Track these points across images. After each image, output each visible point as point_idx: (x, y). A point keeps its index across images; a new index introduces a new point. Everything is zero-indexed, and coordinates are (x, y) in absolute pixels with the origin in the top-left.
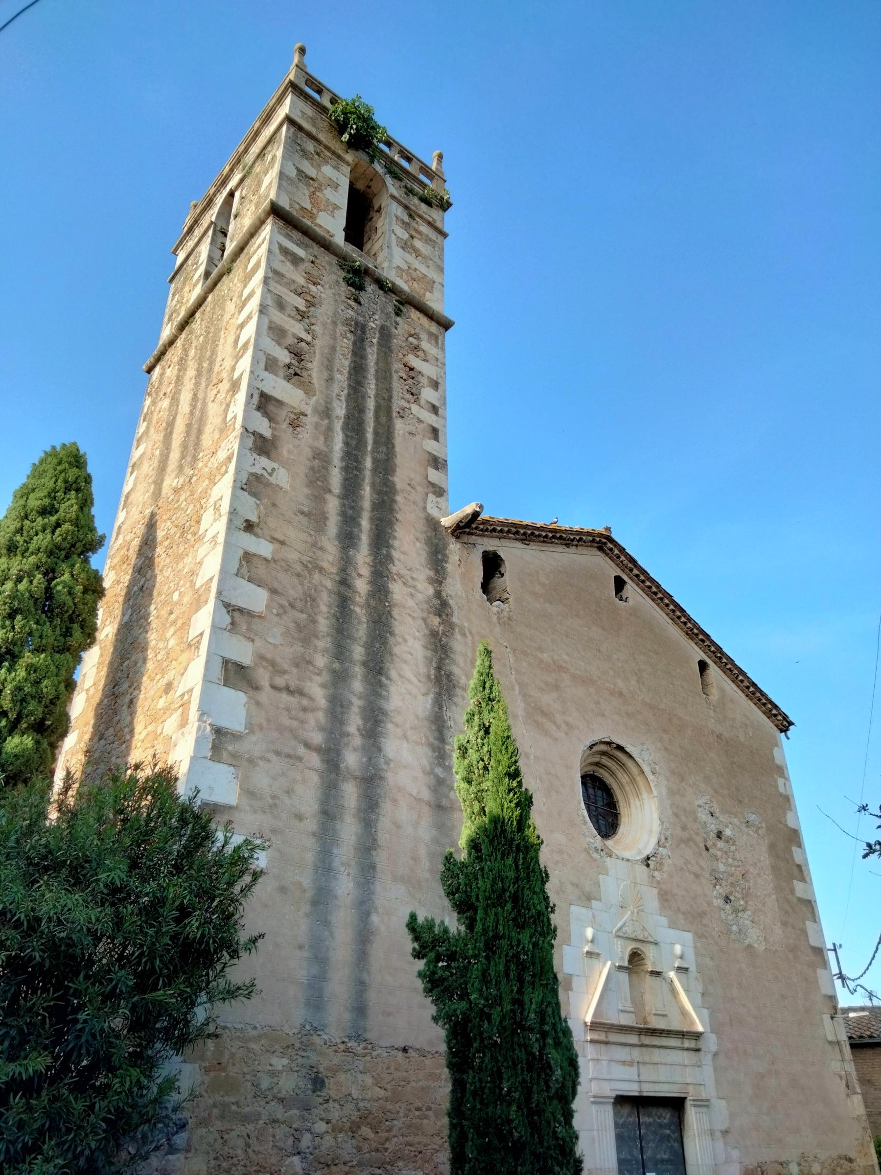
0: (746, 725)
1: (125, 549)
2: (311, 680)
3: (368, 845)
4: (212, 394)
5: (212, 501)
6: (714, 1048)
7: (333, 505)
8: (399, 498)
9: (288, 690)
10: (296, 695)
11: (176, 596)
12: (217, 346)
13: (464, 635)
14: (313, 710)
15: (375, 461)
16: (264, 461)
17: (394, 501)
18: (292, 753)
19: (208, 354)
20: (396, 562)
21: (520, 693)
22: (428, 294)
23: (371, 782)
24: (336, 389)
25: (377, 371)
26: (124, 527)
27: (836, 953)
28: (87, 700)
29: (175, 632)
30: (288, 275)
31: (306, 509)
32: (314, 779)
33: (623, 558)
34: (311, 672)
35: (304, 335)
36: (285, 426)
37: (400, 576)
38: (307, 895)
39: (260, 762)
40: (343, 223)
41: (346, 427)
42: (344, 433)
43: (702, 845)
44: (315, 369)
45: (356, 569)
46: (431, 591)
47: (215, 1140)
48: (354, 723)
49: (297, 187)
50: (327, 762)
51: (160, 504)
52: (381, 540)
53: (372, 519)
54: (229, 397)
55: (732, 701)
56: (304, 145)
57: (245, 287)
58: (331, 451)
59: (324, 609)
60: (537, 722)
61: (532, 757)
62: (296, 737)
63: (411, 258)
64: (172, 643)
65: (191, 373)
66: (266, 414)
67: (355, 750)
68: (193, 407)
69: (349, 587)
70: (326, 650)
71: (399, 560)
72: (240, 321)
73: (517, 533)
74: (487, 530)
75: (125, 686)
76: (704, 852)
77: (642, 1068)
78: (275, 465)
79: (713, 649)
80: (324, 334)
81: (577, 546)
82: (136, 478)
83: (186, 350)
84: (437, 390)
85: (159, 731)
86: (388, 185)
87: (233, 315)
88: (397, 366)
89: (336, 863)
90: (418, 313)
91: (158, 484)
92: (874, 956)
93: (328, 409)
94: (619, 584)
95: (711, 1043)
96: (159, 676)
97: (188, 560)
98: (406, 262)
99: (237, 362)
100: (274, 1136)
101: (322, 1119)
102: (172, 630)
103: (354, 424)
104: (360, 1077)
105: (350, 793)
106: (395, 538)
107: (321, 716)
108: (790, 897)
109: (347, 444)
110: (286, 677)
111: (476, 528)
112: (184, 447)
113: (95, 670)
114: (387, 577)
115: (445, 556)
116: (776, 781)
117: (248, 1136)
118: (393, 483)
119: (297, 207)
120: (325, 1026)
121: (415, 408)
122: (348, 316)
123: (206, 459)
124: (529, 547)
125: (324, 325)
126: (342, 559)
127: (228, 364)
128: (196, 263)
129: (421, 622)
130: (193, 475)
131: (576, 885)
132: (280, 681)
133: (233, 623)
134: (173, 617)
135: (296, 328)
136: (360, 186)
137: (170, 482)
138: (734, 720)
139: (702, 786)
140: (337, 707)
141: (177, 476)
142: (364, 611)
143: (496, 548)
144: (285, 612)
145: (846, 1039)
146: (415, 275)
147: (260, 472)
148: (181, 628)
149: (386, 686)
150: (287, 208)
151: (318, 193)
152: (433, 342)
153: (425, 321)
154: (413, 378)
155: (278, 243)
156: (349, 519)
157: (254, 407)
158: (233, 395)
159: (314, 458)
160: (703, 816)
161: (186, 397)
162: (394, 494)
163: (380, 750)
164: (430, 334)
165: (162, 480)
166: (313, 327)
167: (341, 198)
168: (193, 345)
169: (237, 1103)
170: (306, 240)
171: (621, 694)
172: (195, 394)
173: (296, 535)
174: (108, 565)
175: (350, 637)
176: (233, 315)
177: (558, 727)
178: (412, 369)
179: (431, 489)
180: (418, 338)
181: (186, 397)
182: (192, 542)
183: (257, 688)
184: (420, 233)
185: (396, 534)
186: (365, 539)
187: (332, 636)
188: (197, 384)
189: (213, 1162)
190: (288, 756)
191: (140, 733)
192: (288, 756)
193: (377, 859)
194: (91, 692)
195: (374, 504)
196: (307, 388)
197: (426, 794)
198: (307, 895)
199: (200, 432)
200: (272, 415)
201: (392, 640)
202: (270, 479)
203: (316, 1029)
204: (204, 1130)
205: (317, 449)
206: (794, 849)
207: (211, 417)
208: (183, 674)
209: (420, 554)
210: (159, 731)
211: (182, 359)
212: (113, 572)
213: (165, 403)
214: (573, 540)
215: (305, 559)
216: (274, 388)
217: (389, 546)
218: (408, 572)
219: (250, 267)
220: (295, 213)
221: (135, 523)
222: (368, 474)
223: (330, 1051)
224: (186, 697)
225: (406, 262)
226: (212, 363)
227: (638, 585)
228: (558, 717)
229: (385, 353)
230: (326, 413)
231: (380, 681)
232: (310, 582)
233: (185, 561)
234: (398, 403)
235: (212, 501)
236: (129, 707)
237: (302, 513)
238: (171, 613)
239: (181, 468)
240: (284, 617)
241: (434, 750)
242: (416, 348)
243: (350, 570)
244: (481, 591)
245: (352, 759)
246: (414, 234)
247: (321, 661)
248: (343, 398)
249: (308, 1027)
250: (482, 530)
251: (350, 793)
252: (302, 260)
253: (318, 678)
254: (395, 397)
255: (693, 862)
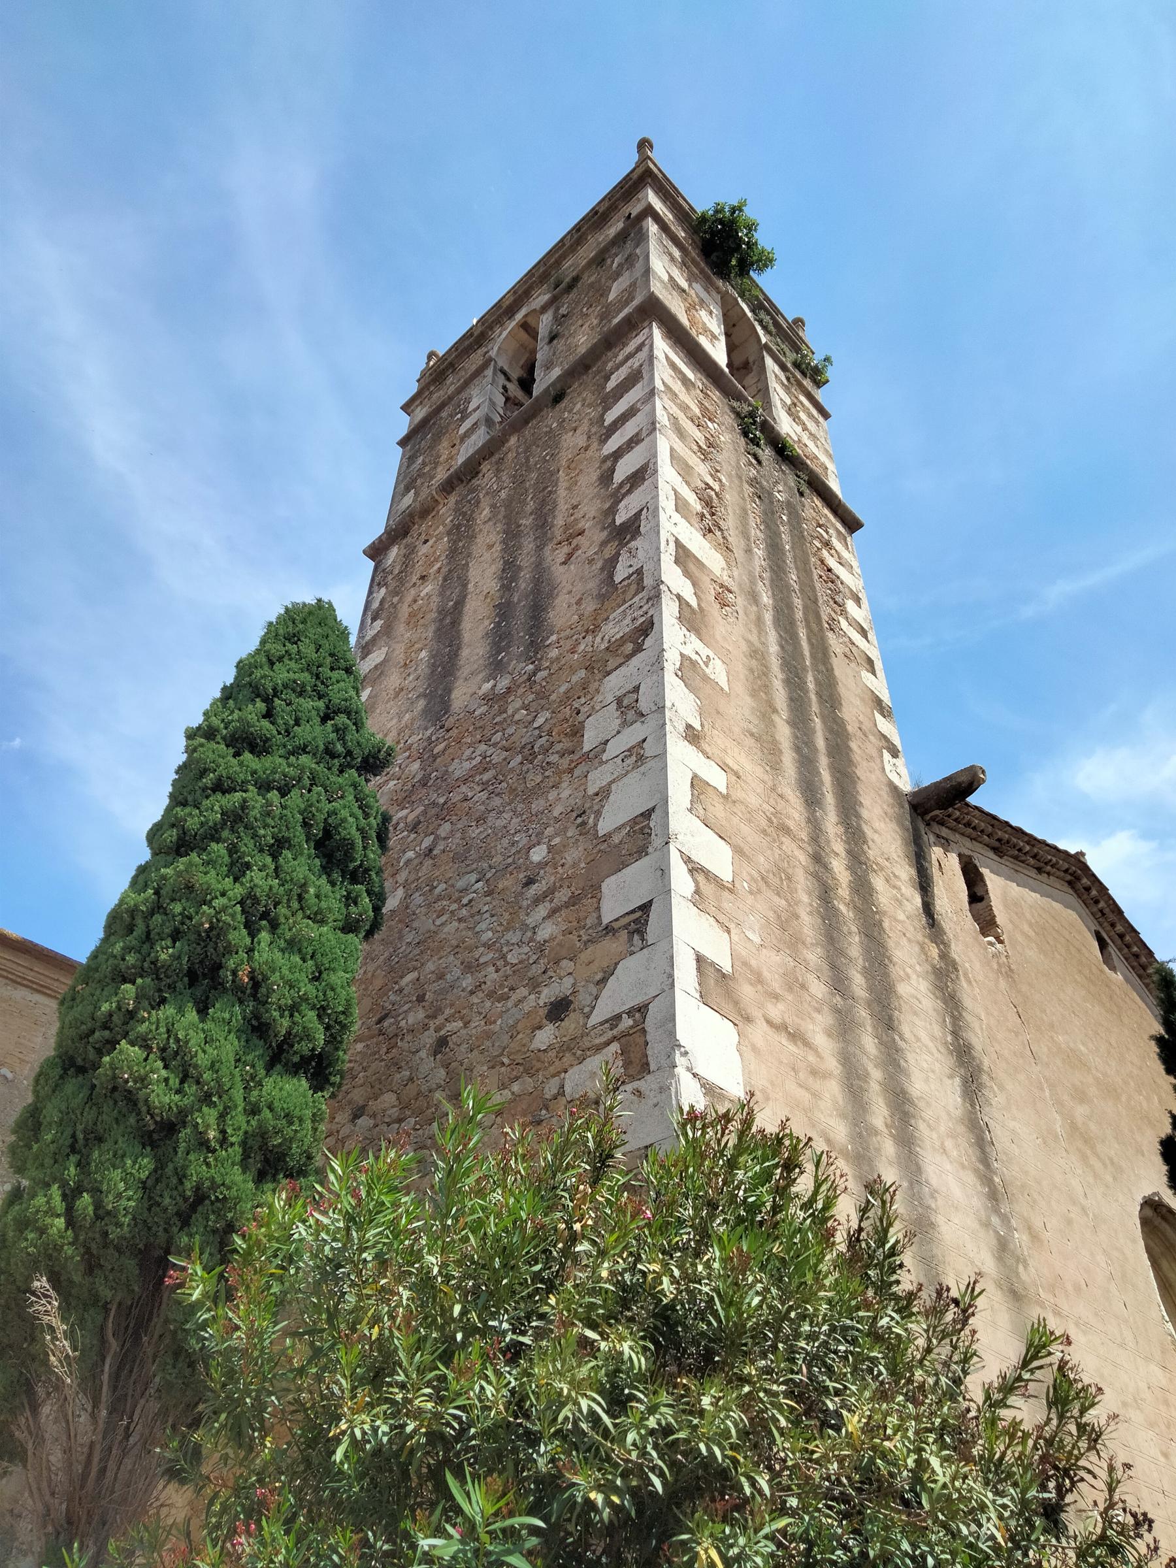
7: (784, 733)
20: (870, 843)
25: (795, 557)
41: (777, 621)
48: (880, 1115)
59: (805, 898)
90: (818, 502)
124: (1002, 861)
129: (917, 949)
133: (697, 892)
149: (902, 1050)
156: (806, 763)
174: (450, 1117)
183: (748, 1019)
186: (830, 799)
187: (822, 946)
202: (707, 671)
227: (1120, 950)
234: (825, 612)
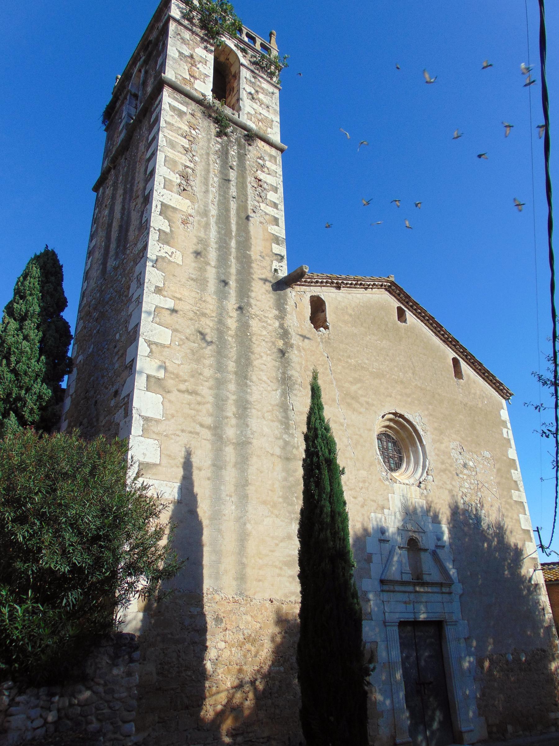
0: (483, 397)
1: (87, 307)
2: (202, 385)
3: (243, 484)
4: (133, 205)
5: (135, 275)
6: (460, 592)
8: (254, 265)
9: (187, 391)
10: (194, 395)
11: (117, 336)
12: (135, 173)
13: (300, 351)
14: (204, 404)
15: (238, 243)
16: (167, 248)
17: (251, 267)
18: (193, 430)
19: (130, 179)
20: (254, 307)
21: (336, 385)
22: (269, 130)
23: (243, 444)
24: (211, 196)
26: (87, 292)
27: (539, 532)
28: (72, 401)
29: (118, 358)
30: (176, 124)
31: (193, 276)
32: (208, 446)
33: (402, 295)
34: (202, 380)
35: (188, 164)
36: (179, 223)
37: (257, 316)
38: (207, 515)
39: (173, 436)
40: (211, 86)
42: (217, 225)
43: (454, 473)
44: (197, 184)
45: (228, 313)
46: (277, 324)
47: (160, 654)
48: (231, 409)
49: (179, 64)
50: (214, 435)
51: (106, 278)
52: (244, 291)
53: (237, 281)
54: (143, 207)
55: (474, 382)
56: (182, 35)
57: (150, 134)
58: (209, 238)
60: (349, 405)
61: (345, 425)
62: (194, 421)
63: (255, 106)
64: (117, 366)
65: (120, 191)
66: (166, 218)
67: (232, 427)
68: (123, 214)
69: (224, 325)
70: (211, 366)
71: (255, 305)
72: (148, 156)
73: (332, 283)
74: (312, 283)
75: (92, 393)
76: (456, 477)
77: (415, 605)
78: (174, 250)
79: (454, 343)
80: (201, 161)
81: (372, 289)
82: (92, 261)
83: (117, 177)
84: (277, 193)
85: (112, 420)
86: (240, 57)
87: (143, 153)
88: (250, 179)
89: (223, 495)
90: (262, 143)
91: (104, 264)
92: (553, 531)
93: (205, 210)
94: (401, 314)
95: (458, 588)
96: (111, 386)
97: (123, 313)
98: (254, 109)
99: (146, 184)
100: (194, 651)
101: (222, 641)
102: (116, 358)
103: (223, 219)
104: (244, 617)
105: (230, 453)
106: (252, 291)
107: (209, 406)
108: (509, 500)
109: (219, 233)
110: (187, 384)
111: (305, 282)
112: (119, 240)
113: (74, 383)
114: (248, 317)
115: (286, 300)
116: (502, 430)
117: (179, 651)
118: (250, 256)
119: (180, 78)
120: (221, 589)
121: (263, 206)
122: (217, 149)
123: (131, 248)
125: (201, 155)
126: (219, 307)
127: (141, 185)
128: (121, 118)
130: (124, 258)
131: (374, 501)
132: (183, 387)
133: (151, 352)
134: (116, 350)
135: (184, 160)
136: (222, 59)
137: (111, 263)
138: (475, 394)
139: (454, 436)
140: (219, 404)
141: (115, 260)
142: (234, 340)
143: (319, 294)
144: (184, 343)
145: (544, 582)
146: (260, 117)
147: (164, 255)
148: (121, 356)
150: (174, 79)
151: (194, 68)
152: (273, 161)
153: (267, 147)
154: (261, 186)
155: (169, 104)
157: (158, 213)
158: (145, 206)
159: (198, 243)
160: (454, 454)
161: (118, 208)
162: (251, 263)
163: (247, 426)
164: (271, 156)
165: (107, 263)
166: (194, 157)
167: (209, 70)
168: (121, 173)
169: (172, 634)
170: (187, 100)
171: (402, 382)
172: (123, 206)
173: (188, 294)
175: (226, 356)
176: (143, 153)
177: (362, 405)
178: (260, 180)
179: (275, 257)
180: (264, 160)
181: (118, 208)
182: (125, 302)
184: (262, 89)
185: (252, 289)
188: (124, 199)
189: (159, 666)
190: (191, 432)
191: (102, 422)
192: (191, 432)
193: (248, 492)
194: (74, 397)
195: (237, 270)
196: (192, 198)
197: (278, 451)
198: (207, 515)
199: (127, 230)
200: (170, 218)
201: (253, 357)
202: (171, 259)
203: (216, 591)
204: (153, 649)
205: (199, 237)
206: (513, 471)
207: (133, 220)
208: (123, 385)
209: (269, 301)
210: (112, 420)
211: (114, 182)
212: (82, 321)
213: (106, 212)
214: (369, 285)
215: (194, 308)
216: (171, 200)
217: (249, 297)
218: (262, 313)
219: (152, 120)
220: (178, 83)
221: (92, 290)
222: (233, 250)
223: (225, 603)
224: (126, 399)
225: (254, 109)
226: (132, 185)
228: (362, 400)
229: (242, 171)
230: (205, 213)
231: (246, 383)
232: (199, 324)
233: (122, 314)
235: (135, 275)
236: (95, 405)
237: (192, 279)
238: (115, 347)
239: (117, 254)
240: (183, 346)
241: (282, 424)
242: (263, 166)
243: (224, 314)
244: (309, 322)
245: (230, 432)
246: (258, 89)
247: (208, 372)
248: (216, 204)
249: (211, 590)
250: (309, 283)
251: (230, 453)
252: (185, 113)
253: (207, 383)
254: (249, 199)
255: (448, 483)
